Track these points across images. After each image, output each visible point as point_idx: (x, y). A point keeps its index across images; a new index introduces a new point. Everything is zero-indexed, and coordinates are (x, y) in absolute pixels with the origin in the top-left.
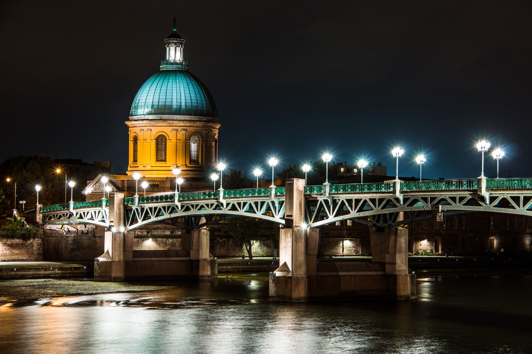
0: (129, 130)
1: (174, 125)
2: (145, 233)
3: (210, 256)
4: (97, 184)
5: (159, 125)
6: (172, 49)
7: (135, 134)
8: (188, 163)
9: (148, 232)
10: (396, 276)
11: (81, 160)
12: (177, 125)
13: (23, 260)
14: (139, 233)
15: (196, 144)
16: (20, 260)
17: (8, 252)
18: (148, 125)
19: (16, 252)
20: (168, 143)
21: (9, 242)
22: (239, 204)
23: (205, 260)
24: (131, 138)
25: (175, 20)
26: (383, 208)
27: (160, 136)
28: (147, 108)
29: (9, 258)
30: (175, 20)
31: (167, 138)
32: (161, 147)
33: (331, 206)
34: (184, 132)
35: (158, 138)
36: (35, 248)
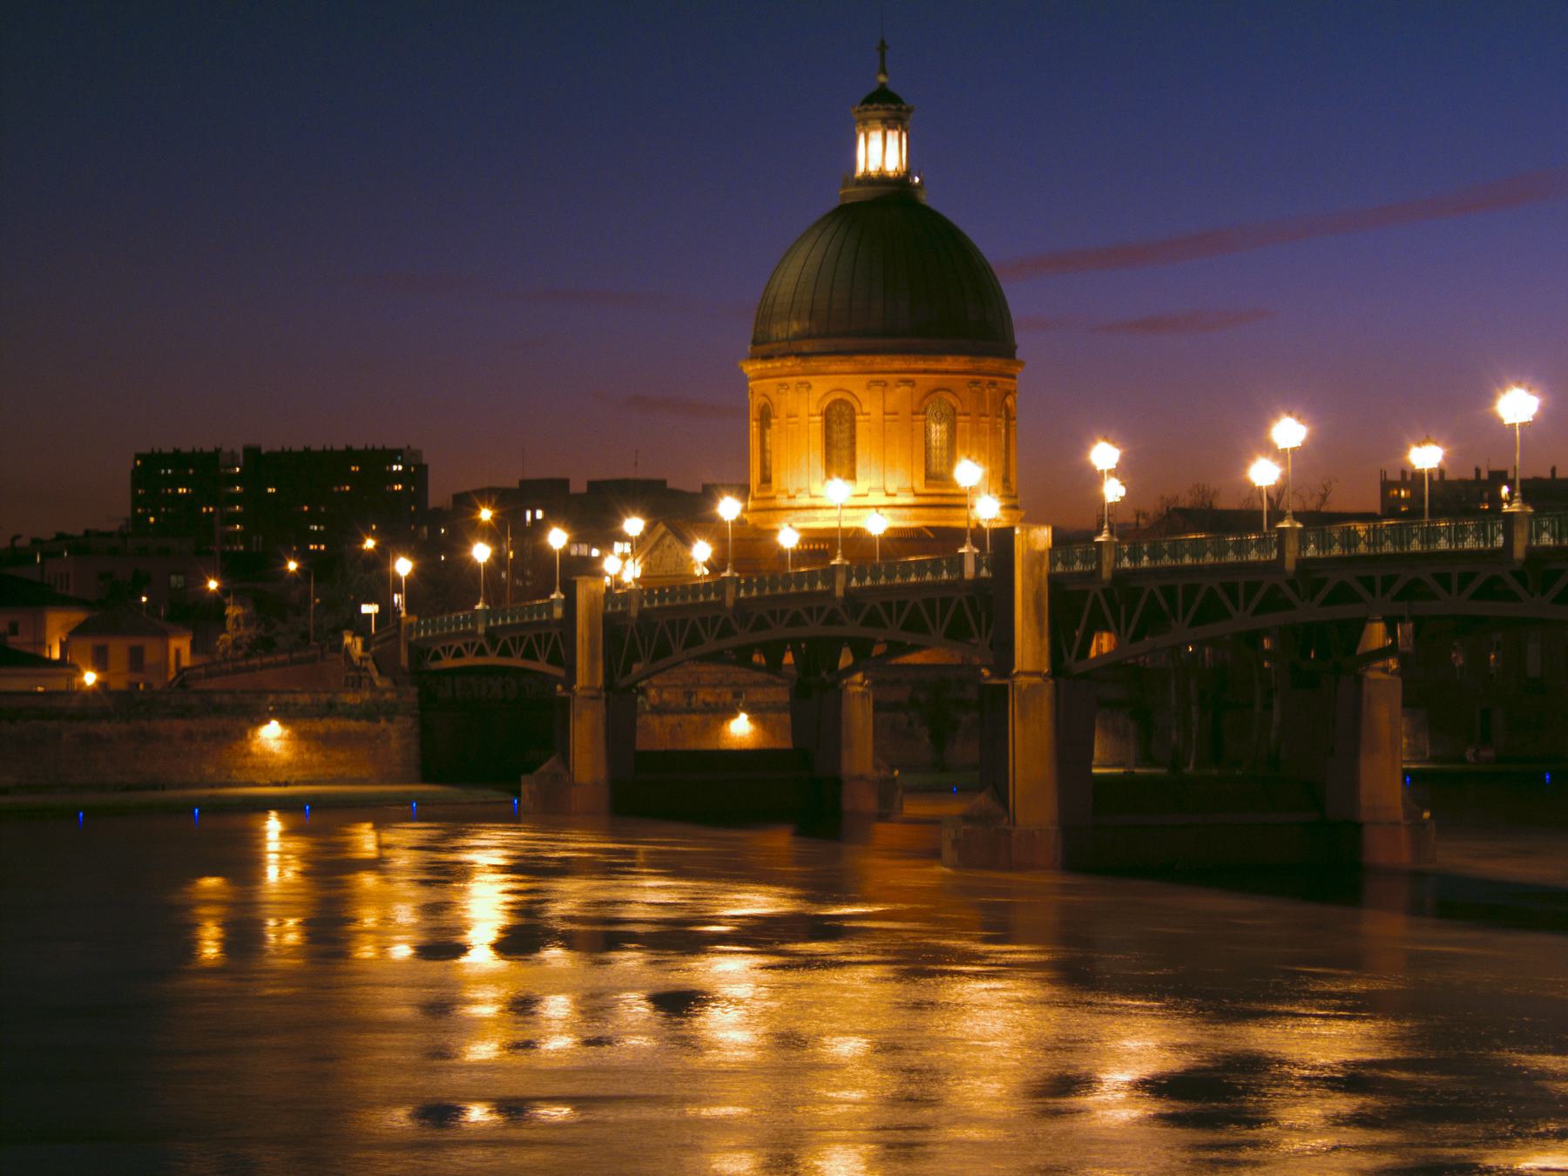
0: (747, 388)
1: (877, 367)
2: (729, 697)
3: (876, 767)
4: (657, 553)
5: (833, 368)
6: (876, 137)
7: (764, 400)
8: (921, 489)
9: (737, 695)
10: (1359, 826)
11: (566, 482)
12: (886, 367)
13: (364, 781)
14: (709, 699)
15: (944, 427)
16: (352, 782)
17: (316, 758)
18: (799, 369)
19: (342, 756)
20: (859, 425)
21: (320, 727)
22: (466, 646)
23: (861, 778)
24: (754, 412)
25: (883, 47)
26: (1257, 612)
27: (835, 402)
28: (798, 319)
29: (299, 774)
30: (883, 47)
31: (858, 410)
32: (841, 436)
33: (1123, 608)
34: (905, 389)
35: (829, 409)
36: (394, 745)
